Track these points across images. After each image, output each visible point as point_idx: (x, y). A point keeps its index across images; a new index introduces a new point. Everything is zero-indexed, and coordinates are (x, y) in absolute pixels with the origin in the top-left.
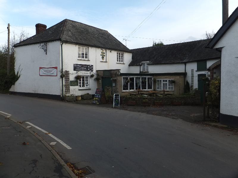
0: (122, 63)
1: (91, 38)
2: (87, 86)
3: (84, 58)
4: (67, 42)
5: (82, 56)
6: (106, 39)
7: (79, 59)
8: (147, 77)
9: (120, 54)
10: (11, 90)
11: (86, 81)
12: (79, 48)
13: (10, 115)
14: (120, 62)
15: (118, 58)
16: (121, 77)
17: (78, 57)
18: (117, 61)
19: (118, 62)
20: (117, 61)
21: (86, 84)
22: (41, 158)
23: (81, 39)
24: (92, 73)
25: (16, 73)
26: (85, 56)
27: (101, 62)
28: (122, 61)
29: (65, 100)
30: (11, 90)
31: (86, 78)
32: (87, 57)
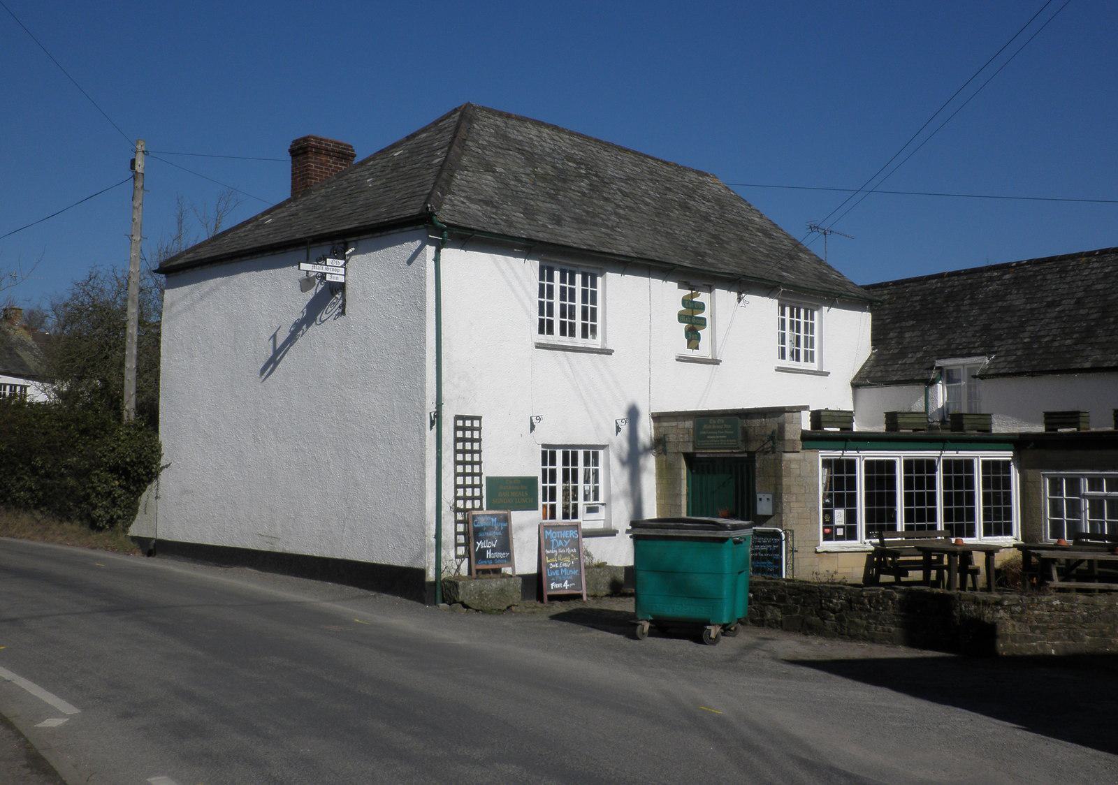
0: (814, 366)
1: (616, 214)
2: (592, 510)
3: (572, 334)
4: (468, 238)
5: (563, 325)
6: (706, 218)
7: (545, 339)
8: (979, 457)
9: (795, 326)
10: (138, 528)
11: (587, 481)
12: (546, 273)
13: (72, 710)
14: (798, 359)
15: (783, 321)
16: (809, 454)
17: (541, 331)
18: (776, 353)
19: (788, 363)
20: (783, 357)
21: (586, 498)
22: (975, 377)
23: (558, 221)
24: (18, 322)
25: (826, 470)
26: (578, 321)
27: (680, 359)
28: (809, 357)
29: (455, 602)
30: (138, 528)
31: (587, 463)
32: (594, 328)
